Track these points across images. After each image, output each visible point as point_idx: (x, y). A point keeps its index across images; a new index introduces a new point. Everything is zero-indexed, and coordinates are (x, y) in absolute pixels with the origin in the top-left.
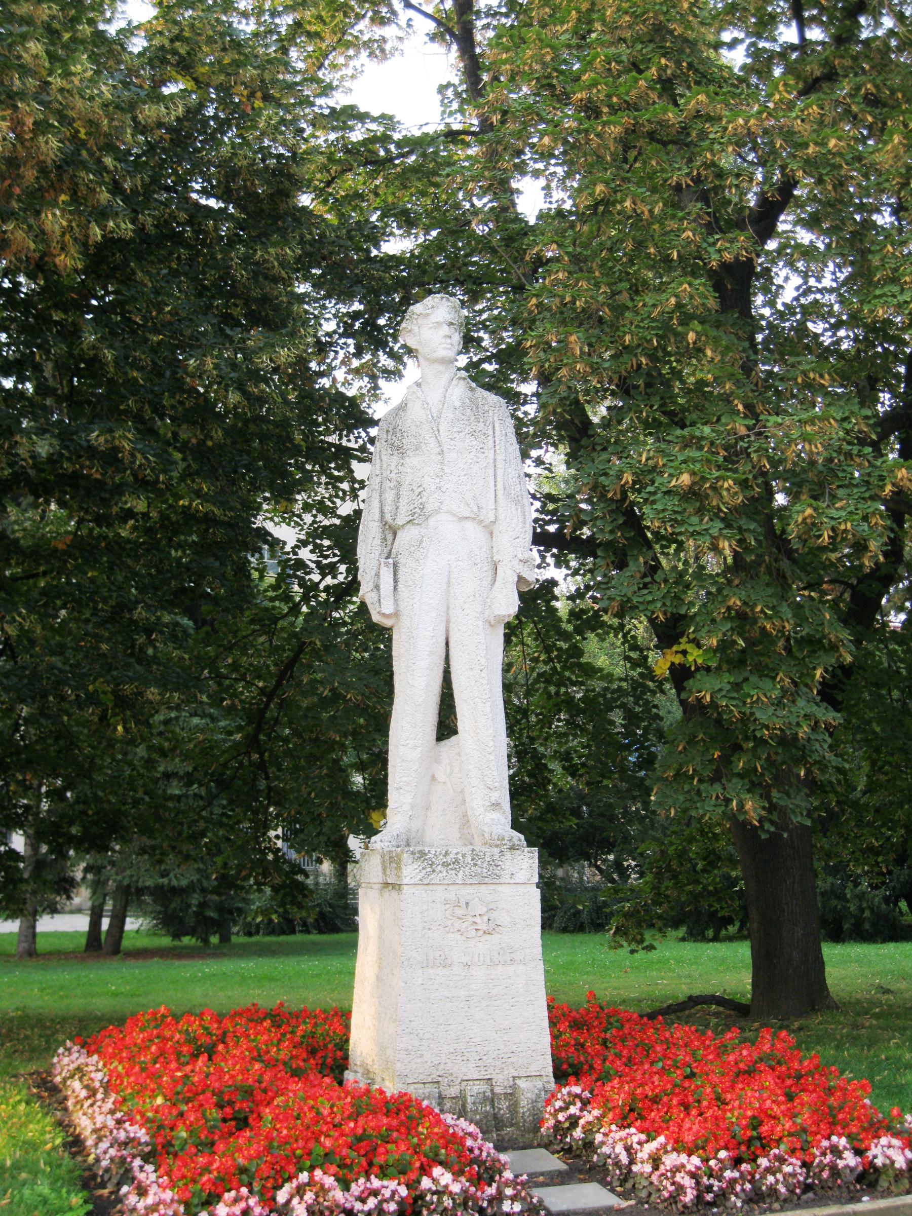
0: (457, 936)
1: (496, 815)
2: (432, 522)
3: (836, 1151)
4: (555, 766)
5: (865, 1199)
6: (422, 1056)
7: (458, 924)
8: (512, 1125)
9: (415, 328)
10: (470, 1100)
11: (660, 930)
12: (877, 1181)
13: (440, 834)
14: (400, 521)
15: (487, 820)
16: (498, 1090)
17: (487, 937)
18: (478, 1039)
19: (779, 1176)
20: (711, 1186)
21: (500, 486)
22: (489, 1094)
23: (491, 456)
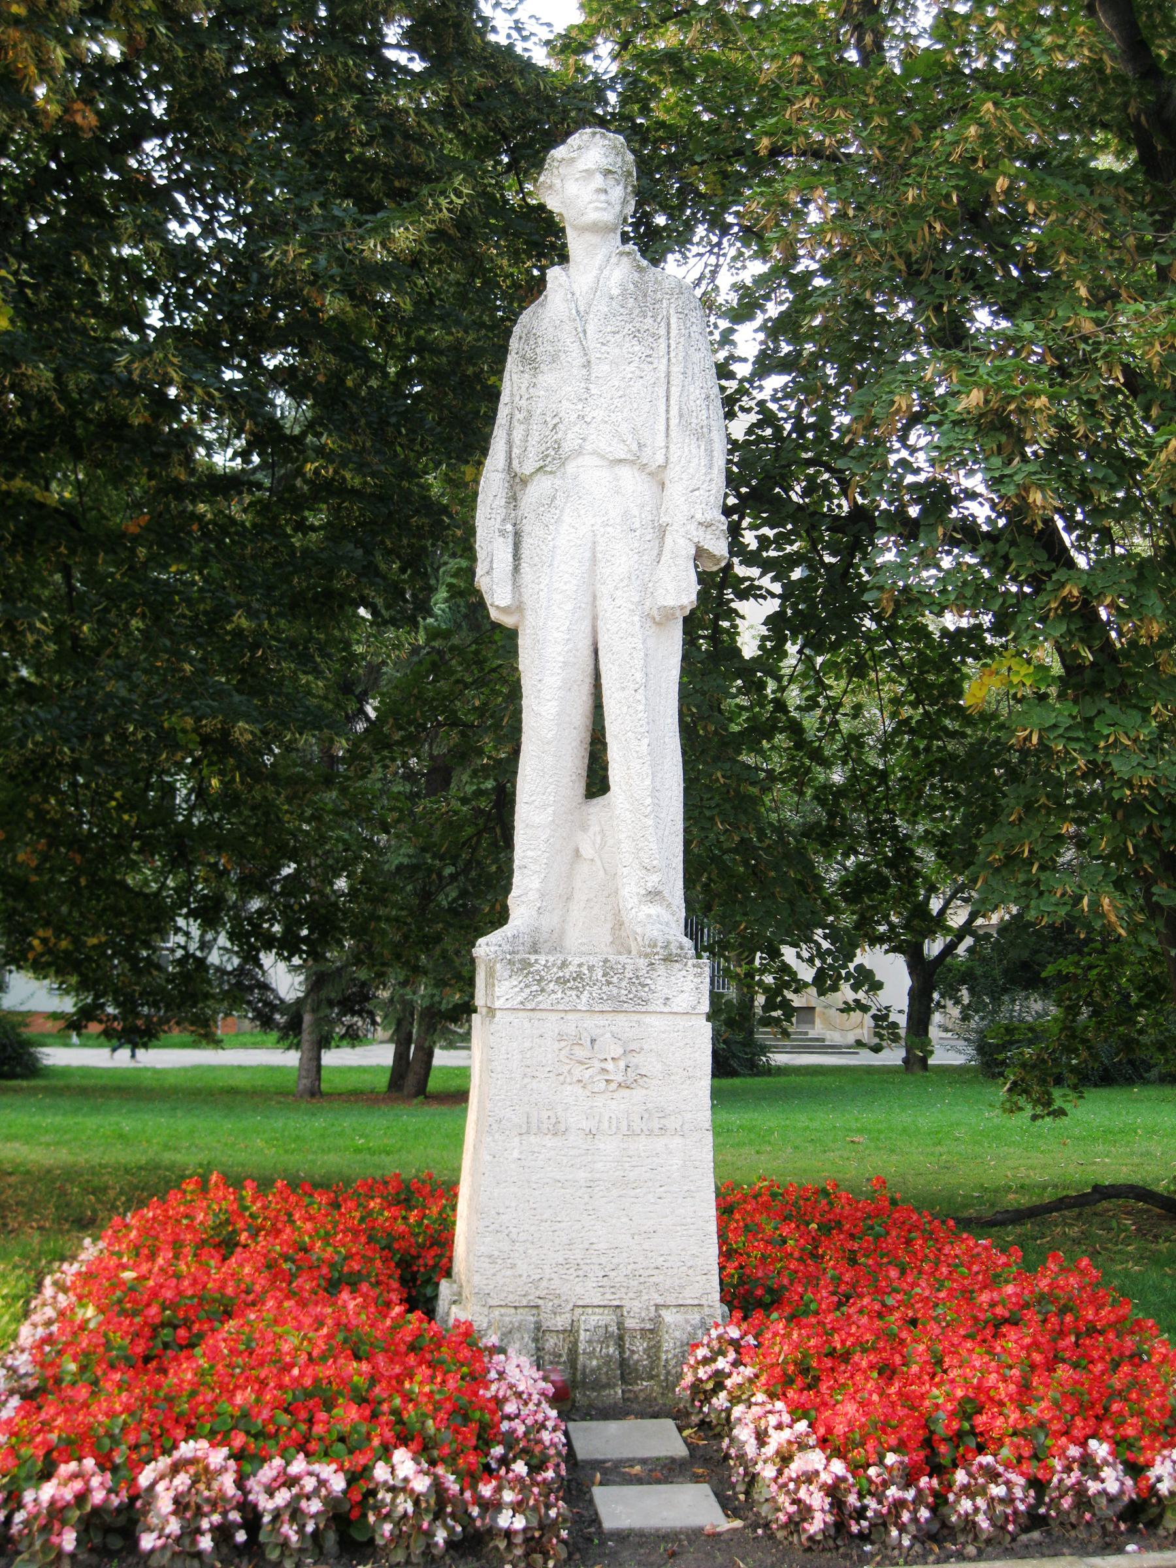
0: (578, 1089)
1: (654, 910)
2: (571, 468)
3: (1089, 1465)
4: (927, 855)
5: (1130, 1548)
6: (513, 1266)
7: (578, 1071)
8: (651, 1377)
9: (557, 181)
10: (583, 1336)
11: (1075, 1088)
12: (1161, 1516)
13: (584, 939)
14: (528, 468)
15: (641, 916)
16: (630, 1323)
17: (625, 1092)
18: (602, 1246)
19: (981, 1502)
20: (865, 1508)
21: (674, 411)
22: (613, 1329)
23: (663, 367)
